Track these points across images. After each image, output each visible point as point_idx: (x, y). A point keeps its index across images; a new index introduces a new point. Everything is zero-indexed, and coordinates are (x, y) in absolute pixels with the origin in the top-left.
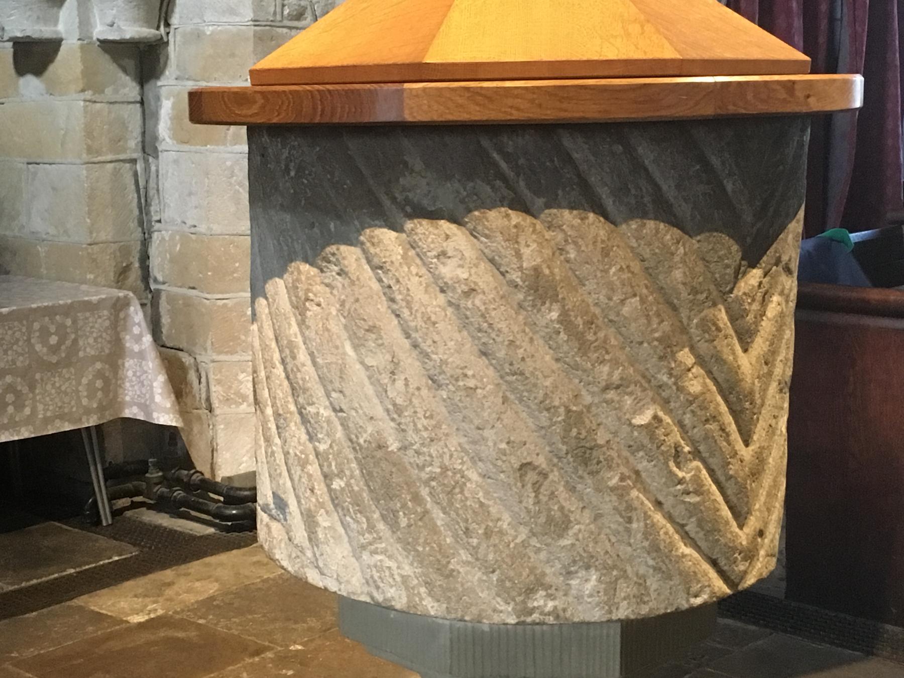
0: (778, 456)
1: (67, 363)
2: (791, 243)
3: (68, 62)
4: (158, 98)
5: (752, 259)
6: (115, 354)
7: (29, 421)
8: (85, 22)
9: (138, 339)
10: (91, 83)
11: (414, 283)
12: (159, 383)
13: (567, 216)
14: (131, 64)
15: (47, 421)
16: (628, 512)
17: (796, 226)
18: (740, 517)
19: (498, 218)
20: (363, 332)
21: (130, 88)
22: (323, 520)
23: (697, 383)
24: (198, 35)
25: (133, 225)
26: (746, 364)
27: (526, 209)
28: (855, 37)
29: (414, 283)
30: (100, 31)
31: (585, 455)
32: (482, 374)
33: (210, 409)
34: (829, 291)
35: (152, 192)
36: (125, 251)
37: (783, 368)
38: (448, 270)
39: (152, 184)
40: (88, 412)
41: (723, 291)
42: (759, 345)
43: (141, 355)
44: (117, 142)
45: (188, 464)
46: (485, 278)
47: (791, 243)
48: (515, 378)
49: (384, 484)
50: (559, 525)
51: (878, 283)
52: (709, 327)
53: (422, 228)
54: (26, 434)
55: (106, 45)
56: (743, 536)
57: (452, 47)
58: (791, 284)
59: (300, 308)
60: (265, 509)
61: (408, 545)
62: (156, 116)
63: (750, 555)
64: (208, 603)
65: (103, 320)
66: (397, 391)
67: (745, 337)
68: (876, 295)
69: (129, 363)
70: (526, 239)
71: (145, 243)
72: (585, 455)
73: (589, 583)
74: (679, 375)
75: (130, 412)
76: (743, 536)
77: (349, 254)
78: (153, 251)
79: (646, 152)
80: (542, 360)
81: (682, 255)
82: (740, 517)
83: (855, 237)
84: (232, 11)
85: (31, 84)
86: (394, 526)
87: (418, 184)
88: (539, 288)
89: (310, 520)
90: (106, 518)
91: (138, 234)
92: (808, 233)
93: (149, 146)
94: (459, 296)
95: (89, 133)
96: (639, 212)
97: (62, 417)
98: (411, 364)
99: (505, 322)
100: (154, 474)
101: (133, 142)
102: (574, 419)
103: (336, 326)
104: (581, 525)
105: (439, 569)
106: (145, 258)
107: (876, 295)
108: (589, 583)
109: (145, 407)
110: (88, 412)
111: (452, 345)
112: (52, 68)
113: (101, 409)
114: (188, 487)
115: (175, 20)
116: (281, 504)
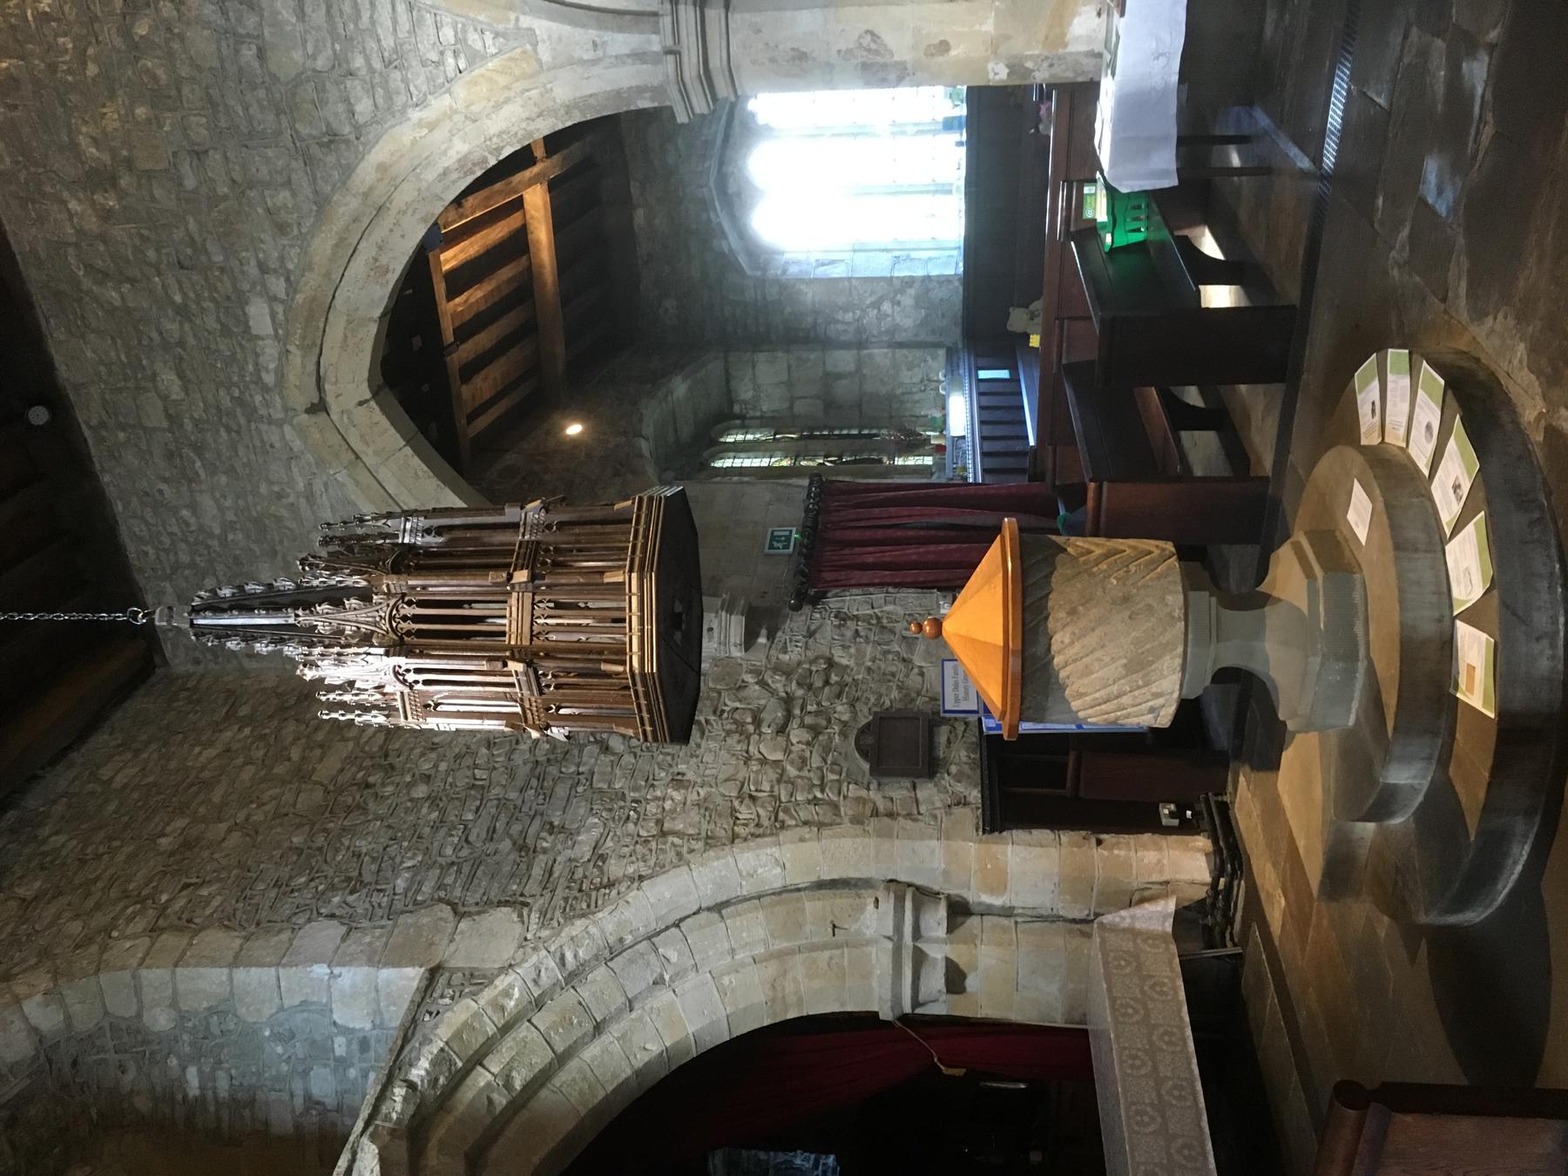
0: (1132, 542)
1: (1137, 958)
2: (1060, 540)
3: (959, 954)
4: (980, 904)
5: (1065, 550)
6: (1133, 933)
7: (1173, 980)
8: (937, 941)
9: (1123, 918)
10: (971, 940)
11: (1072, 652)
12: (1149, 908)
13: (1050, 604)
14: (960, 919)
15: (1172, 970)
16: (1146, 586)
17: (1054, 537)
18: (1150, 553)
19: (1051, 624)
20: (1087, 671)
21: (974, 921)
22: (1154, 690)
23: (1103, 566)
24: (946, 873)
25: (1054, 926)
26: (1098, 551)
27: (1047, 618)
28: (939, 515)
29: (1072, 652)
30: (941, 932)
31: (1126, 599)
32: (1099, 631)
33: (1167, 883)
34: (1089, 525)
35: (1035, 913)
36: (1070, 932)
37: (1101, 540)
38: (1067, 641)
39: (1030, 912)
40: (1167, 949)
41: (1075, 559)
42: (1092, 548)
43: (1133, 917)
44: (1005, 930)
45: (1203, 900)
46: (1069, 629)
47: (1060, 540)
48: (1100, 621)
49: (1138, 665)
50: (1150, 608)
51: (1084, 502)
52: (1085, 563)
53: (1054, 648)
54: (1180, 983)
55: (950, 930)
56: (1157, 552)
57: (999, 640)
58: (1073, 539)
59: (1081, 695)
60: (1156, 718)
61: (1159, 657)
62: (990, 906)
63: (1164, 550)
64: (1274, 865)
65: (1111, 937)
66: (1107, 659)
67: (1090, 552)
68: (1090, 503)
69: (1138, 925)
70: (1057, 618)
71: (1066, 920)
72: (1126, 599)
73: (1169, 598)
74: (1101, 571)
75: (1168, 926)
76: (1157, 552)
77: (1062, 674)
78: (1070, 916)
79: (1031, 581)
80: (1094, 613)
81: (1061, 572)
82: (1150, 553)
83: (1062, 512)
84: (933, 852)
85: (971, 983)
86: (1153, 662)
87: (1040, 650)
88: (1073, 612)
89: (1157, 695)
90: (1239, 950)
91: (1061, 924)
92: (1058, 533)
93: (1007, 912)
94: (1076, 638)
95: (1000, 944)
96: (1049, 583)
97: (1171, 963)
98: (1098, 654)
99: (1083, 623)
100: (1210, 920)
101: (1005, 921)
102: (1114, 602)
103: (1086, 681)
104: (1150, 601)
105: (1167, 647)
106: (1074, 921)
107: (1090, 503)
108: (1169, 598)
109: (1165, 917)
110: (1167, 949)
111: (1091, 640)
112: (962, 966)
113: (1166, 942)
114: (1216, 897)
115: (936, 888)
116: (1152, 710)
